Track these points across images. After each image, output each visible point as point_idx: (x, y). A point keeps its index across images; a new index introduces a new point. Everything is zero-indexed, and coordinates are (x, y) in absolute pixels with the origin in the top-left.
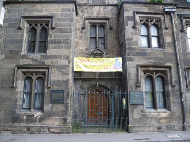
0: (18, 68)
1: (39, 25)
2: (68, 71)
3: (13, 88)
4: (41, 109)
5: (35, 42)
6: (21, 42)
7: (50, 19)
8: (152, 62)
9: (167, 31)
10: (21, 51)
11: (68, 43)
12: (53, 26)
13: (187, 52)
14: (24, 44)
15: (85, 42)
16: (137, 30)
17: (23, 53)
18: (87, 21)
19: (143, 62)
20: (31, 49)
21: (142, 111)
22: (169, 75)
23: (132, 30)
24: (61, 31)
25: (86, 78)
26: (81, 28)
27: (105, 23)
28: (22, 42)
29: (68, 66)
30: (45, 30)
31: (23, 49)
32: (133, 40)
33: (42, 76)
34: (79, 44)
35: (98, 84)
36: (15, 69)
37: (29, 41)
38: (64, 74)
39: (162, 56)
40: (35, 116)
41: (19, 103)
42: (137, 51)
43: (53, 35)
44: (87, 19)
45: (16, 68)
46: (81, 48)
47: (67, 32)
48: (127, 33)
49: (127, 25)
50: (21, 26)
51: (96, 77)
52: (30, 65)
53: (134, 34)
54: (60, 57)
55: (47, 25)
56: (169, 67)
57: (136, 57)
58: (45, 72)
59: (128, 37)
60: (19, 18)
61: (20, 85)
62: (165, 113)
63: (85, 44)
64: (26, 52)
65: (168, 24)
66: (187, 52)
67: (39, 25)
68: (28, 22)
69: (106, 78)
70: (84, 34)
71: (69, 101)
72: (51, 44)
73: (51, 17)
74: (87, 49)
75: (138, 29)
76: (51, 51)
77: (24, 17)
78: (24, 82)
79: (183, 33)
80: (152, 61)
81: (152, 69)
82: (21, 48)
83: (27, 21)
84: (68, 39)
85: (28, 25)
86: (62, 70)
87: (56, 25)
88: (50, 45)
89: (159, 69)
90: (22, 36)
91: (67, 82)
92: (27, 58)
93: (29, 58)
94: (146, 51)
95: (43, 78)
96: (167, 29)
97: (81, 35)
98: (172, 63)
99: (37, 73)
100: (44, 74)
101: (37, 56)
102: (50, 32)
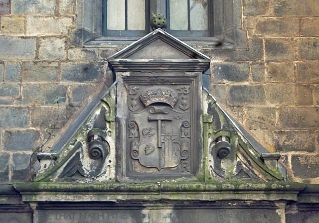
46: (32, 32)
74: (79, 37)
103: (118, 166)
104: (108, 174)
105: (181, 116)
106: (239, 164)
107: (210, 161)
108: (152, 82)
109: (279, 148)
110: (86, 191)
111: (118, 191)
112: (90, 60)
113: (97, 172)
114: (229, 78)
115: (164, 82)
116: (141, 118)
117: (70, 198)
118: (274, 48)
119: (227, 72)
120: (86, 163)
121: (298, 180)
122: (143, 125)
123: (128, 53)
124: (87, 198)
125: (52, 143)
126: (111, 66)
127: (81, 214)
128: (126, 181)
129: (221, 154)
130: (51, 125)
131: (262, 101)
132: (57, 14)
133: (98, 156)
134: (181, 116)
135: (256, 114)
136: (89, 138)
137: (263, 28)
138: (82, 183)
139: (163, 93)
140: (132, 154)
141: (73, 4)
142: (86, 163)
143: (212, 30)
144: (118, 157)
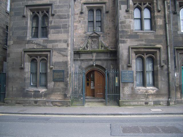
0: (25, 52)
1: (40, 13)
2: (67, 54)
3: (22, 69)
4: (46, 86)
5: (37, 28)
6: (26, 28)
7: (50, 7)
8: (143, 44)
9: (159, 14)
10: (26, 36)
11: (66, 28)
12: (53, 13)
13: (178, 33)
14: (28, 31)
15: (83, 26)
16: (129, 14)
17: (28, 39)
18: (85, 6)
19: (135, 43)
20: (36, 35)
21: (132, 88)
22: (158, 56)
23: (126, 14)
24: (60, 17)
25: (84, 58)
26: (79, 13)
27: (102, 7)
28: (27, 29)
29: (67, 49)
30: (45, 17)
31: (28, 35)
32: (126, 23)
33: (45, 58)
34: (78, 28)
35: (94, 65)
36: (22, 52)
37: (33, 27)
38: (64, 56)
39: (153, 38)
40: (41, 92)
41: (28, 81)
42: (129, 34)
43: (53, 21)
44: (85, 4)
45: (23, 52)
47: (66, 18)
48: (120, 16)
49: (121, 9)
50: (25, 14)
51: (93, 57)
52: (34, 49)
53: (127, 17)
54: (60, 41)
55: (48, 12)
56: (159, 49)
57: (129, 40)
58: (47, 55)
59: (121, 20)
60: (23, 7)
61: (28, 66)
62: (153, 90)
63: (83, 28)
64: (31, 37)
65: (160, 7)
66: (178, 33)
67: (40, 13)
68: (31, 10)
69: (102, 58)
70: (82, 19)
71: (68, 79)
72: (51, 30)
73: (51, 5)
74: (85, 33)
75: (130, 12)
76: (52, 36)
77: (27, 6)
78: (30, 63)
79: (175, 15)
80: (144, 43)
81: (142, 50)
82: (27, 34)
83: (30, 9)
84: (67, 25)
85: (32, 13)
86: (62, 53)
87: (55, 11)
88: (51, 31)
89: (150, 50)
90: (27, 23)
91: (66, 63)
92: (32, 43)
93: (34, 42)
94: (138, 34)
95: (45, 60)
96: (159, 11)
97: (79, 19)
98: (162, 45)
99: (40, 56)
100: (46, 56)
101: (40, 40)
102: (51, 19)
103: (90, 48)
104: (88, 50)
105: (97, 42)
106: (51, 24)
107: (100, 47)
108: (93, 38)
109: (109, 46)
110: (86, 51)
111: (90, 51)
112: (86, 35)
113: (87, 49)
114: (103, 37)
115: (95, 38)
116: (92, 42)
117: (84, 52)
118: (109, 33)
119: (103, 36)
120: (86, 48)
121: (111, 50)
122: (93, 43)
123: (91, 34)
124: (86, 52)
125: (82, 46)
126: (89, 36)
127: (55, 27)
128: (91, 50)
129: (102, 47)
130: (82, 43)
131: (107, 40)
132: (82, 30)
133: (87, 47)
134: (97, 42)
135: (106, 42)
136: (86, 45)
137: (107, 31)
138: (85, 50)
139: (95, 39)
140: (91, 47)
141: (128, 36)
142: (86, 48)
143: (101, 31)
144: (90, 47)
